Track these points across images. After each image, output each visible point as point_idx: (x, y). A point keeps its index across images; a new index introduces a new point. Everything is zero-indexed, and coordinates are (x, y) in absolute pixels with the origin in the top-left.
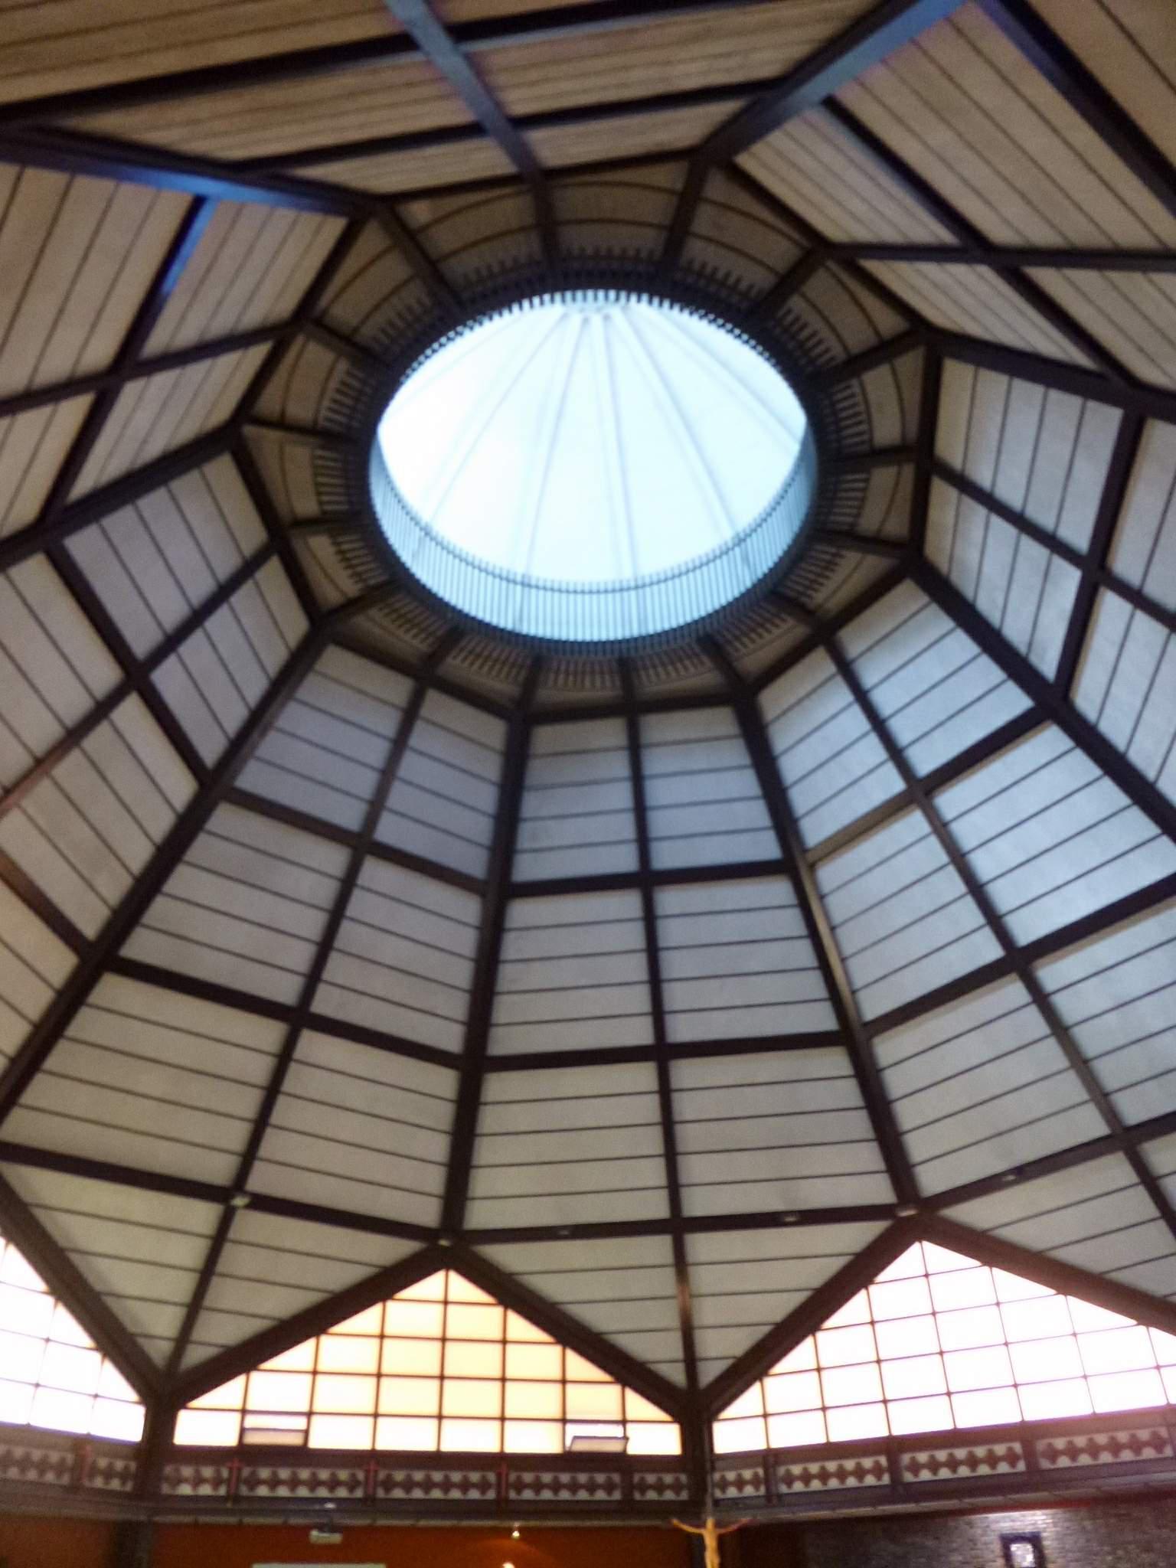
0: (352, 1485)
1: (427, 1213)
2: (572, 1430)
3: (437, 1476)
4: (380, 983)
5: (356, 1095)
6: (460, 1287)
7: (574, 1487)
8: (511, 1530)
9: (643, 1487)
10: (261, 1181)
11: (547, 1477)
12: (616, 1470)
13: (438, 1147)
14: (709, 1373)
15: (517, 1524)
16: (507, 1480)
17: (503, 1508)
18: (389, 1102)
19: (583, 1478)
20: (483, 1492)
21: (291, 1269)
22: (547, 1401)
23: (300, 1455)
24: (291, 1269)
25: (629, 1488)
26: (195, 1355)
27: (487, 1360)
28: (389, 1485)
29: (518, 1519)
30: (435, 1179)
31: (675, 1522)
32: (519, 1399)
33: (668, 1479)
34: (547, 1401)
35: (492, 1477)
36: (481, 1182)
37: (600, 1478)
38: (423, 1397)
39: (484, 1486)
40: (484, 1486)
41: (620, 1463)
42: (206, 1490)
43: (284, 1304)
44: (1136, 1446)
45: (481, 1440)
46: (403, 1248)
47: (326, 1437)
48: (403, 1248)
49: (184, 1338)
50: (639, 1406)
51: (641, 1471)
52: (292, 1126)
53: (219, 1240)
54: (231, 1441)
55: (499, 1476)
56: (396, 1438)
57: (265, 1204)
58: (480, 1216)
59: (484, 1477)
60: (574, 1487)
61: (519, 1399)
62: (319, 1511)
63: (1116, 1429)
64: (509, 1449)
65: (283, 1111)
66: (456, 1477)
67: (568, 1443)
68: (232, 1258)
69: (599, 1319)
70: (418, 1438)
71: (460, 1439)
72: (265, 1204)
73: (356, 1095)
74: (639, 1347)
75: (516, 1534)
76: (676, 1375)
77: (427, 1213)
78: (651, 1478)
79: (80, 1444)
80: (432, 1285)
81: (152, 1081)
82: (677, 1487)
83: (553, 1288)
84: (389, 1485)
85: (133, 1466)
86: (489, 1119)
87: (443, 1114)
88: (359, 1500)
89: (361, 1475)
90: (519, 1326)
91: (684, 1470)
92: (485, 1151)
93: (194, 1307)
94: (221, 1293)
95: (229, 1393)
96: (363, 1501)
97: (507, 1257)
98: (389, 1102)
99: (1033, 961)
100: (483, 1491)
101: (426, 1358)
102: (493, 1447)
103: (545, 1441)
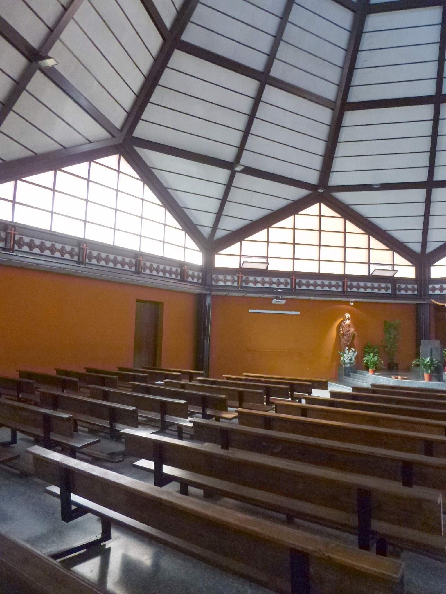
0: (286, 284)
1: (313, 178)
2: (373, 268)
3: (319, 282)
4: (303, 60)
5: (288, 120)
6: (326, 210)
7: (373, 288)
8: (350, 302)
9: (400, 289)
10: (246, 159)
11: (362, 284)
12: (389, 282)
13: (320, 147)
14: (431, 248)
15: (352, 300)
16: (347, 284)
17: (344, 293)
18: (303, 125)
19: (376, 285)
20: (337, 289)
21: (257, 200)
22: (362, 256)
23: (265, 273)
24: (257, 200)
25: (394, 288)
26: (220, 234)
27: (338, 239)
28: (300, 284)
29: (353, 298)
30: (317, 162)
31: (433, 301)
32: (351, 255)
33: (410, 286)
34: (362, 256)
35: (340, 283)
36: (338, 164)
37: (383, 285)
38: (313, 253)
39: (337, 286)
40: (337, 286)
41: (393, 281)
42: (229, 284)
43: (255, 215)
44: (123, 264)
45: (337, 269)
46: (303, 193)
47: (274, 266)
48: (303, 193)
49: (215, 227)
50: (399, 259)
51: (399, 283)
52: (426, 153)
53: (229, 186)
54: (237, 266)
55: (343, 283)
56: (301, 267)
57: (249, 171)
58: (335, 180)
59: (337, 283)
60: (373, 288)
61: (326, 253)
62: (276, 292)
63: (118, 255)
64: (347, 273)
65: (257, 127)
66: (326, 282)
67: (371, 273)
68: (234, 195)
69: (384, 224)
70: (312, 268)
71: (327, 269)
72: (249, 171)
73: (288, 120)
74: (401, 236)
75: (352, 304)
76: (417, 248)
77: (313, 178)
78: (403, 286)
79: (182, 265)
80: (314, 209)
81: (198, 108)
82: (413, 290)
83: (365, 211)
84: (351, 287)
85: (201, 274)
86: (345, 134)
87: (323, 131)
88: (289, 289)
89: (289, 281)
90: (351, 227)
91: (416, 284)
92: (341, 150)
93: (219, 214)
94: (229, 209)
95: (234, 248)
96: (291, 289)
97: (346, 197)
98: (303, 125)
99: (370, 13)
100: (286, 285)
101: (313, 237)
102: (341, 272)
103: (362, 271)
